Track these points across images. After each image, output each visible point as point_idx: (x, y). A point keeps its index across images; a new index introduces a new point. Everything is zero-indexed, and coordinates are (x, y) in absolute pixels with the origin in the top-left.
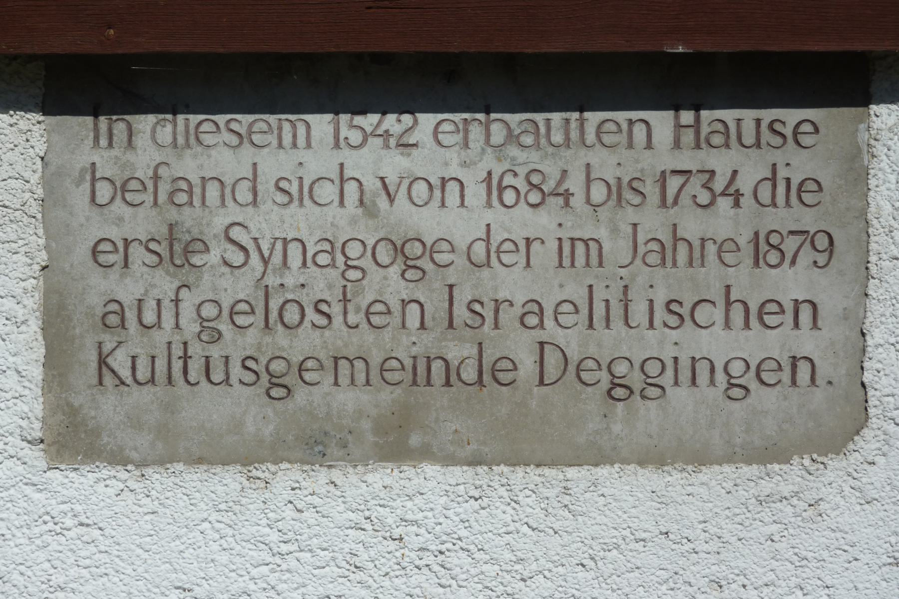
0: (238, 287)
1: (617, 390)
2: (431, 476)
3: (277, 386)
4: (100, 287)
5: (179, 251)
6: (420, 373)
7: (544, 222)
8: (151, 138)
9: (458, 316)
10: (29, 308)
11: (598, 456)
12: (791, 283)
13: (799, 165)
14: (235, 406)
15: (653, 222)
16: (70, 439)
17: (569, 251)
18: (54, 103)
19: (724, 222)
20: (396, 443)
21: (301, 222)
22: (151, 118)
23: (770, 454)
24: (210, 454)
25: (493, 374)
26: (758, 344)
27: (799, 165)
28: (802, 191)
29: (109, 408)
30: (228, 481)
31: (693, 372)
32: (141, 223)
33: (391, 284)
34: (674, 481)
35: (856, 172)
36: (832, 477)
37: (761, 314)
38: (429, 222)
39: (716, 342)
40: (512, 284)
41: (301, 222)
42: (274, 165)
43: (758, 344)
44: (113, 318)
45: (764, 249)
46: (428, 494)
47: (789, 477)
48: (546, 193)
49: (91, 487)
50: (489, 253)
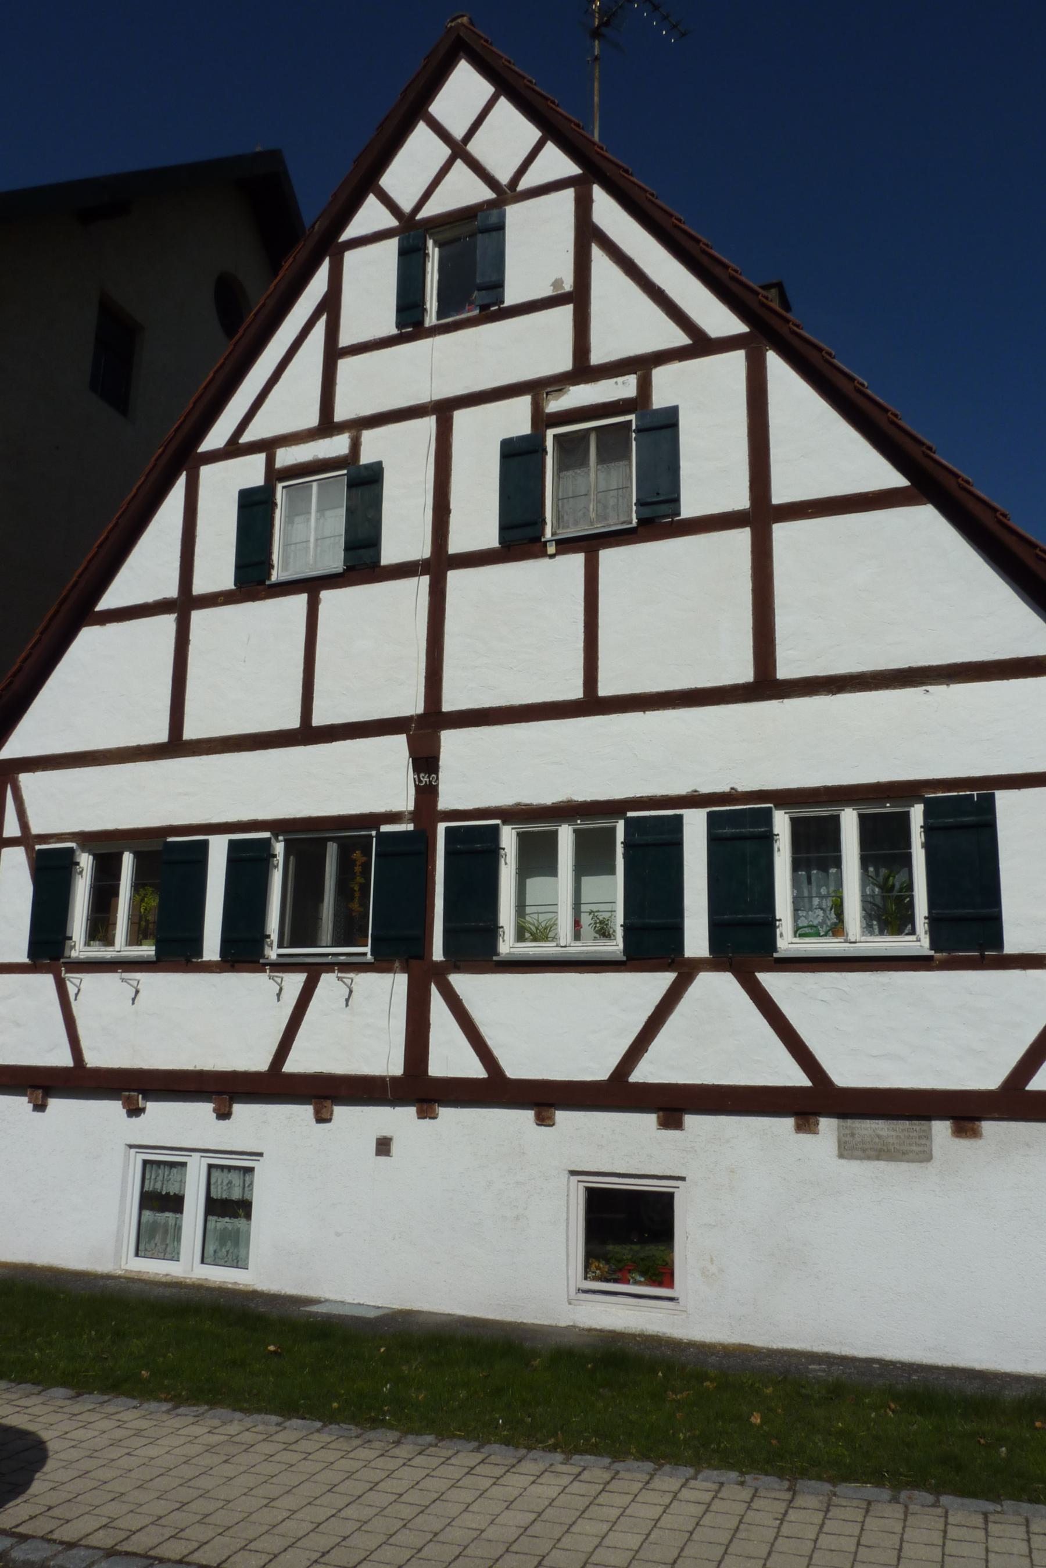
0: (859, 1140)
1: (903, 1153)
2: (882, 1163)
3: (864, 1151)
4: (844, 1139)
5: (853, 1135)
6: (881, 1150)
7: (894, 1133)
8: (849, 1122)
9: (603, 517)
10: (836, 1141)
11: (901, 1161)
12: (923, 1142)
13: (924, 1128)
14: (859, 1153)
15: (906, 1134)
16: (841, 1156)
17: (897, 1137)
18: (838, 1118)
19: (915, 1134)
20: (878, 1158)
21: (866, 1132)
22: (215, 1218)
23: (921, 1162)
24: (857, 1158)
25: (888, 1151)
26: (921, 1149)
27: (924, 1128)
28: (924, 1131)
29: (845, 1153)
30: (859, 1162)
31: (912, 1151)
32: (848, 1132)
33: (877, 1140)
34: (911, 1164)
35: (930, 1129)
36: (929, 1164)
37: (920, 1145)
38: (881, 1133)
39: (914, 1148)
40: (891, 1140)
41: (866, 1132)
42: (863, 1126)
43: (921, 1149)
44: (845, 1142)
45: (920, 1137)
46: (882, 1164)
47: (923, 1164)
48: (894, 1130)
49: (843, 1162)
50: (888, 1136)
